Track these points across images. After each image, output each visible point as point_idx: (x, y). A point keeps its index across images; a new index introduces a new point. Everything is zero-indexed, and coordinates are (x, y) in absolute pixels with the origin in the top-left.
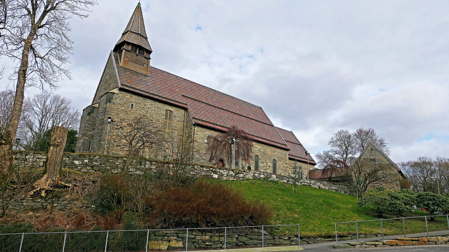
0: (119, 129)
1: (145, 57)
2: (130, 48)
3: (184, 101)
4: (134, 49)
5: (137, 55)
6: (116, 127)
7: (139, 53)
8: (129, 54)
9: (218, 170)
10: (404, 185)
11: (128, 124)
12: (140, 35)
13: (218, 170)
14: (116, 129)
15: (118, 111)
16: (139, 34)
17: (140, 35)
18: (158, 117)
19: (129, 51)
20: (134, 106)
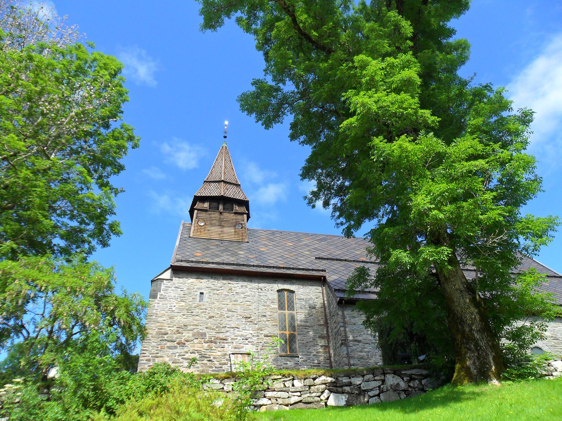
0: (175, 347)
1: (235, 213)
2: (206, 205)
3: (321, 265)
4: (215, 204)
5: (221, 213)
6: (169, 344)
7: (224, 209)
8: (203, 215)
9: (345, 380)
10: (452, 213)
11: (194, 335)
12: (225, 182)
13: (345, 380)
14: (169, 348)
15: (173, 311)
16: (223, 181)
17: (225, 182)
18: (261, 308)
19: (206, 211)
20: (206, 295)
